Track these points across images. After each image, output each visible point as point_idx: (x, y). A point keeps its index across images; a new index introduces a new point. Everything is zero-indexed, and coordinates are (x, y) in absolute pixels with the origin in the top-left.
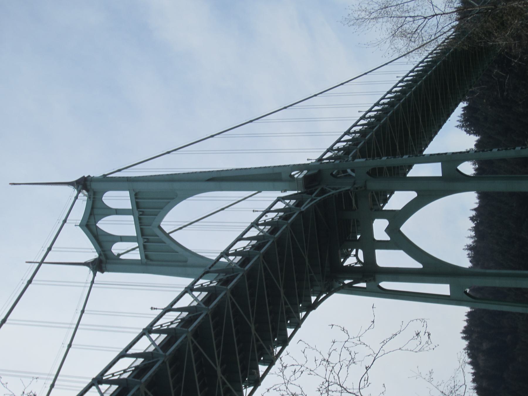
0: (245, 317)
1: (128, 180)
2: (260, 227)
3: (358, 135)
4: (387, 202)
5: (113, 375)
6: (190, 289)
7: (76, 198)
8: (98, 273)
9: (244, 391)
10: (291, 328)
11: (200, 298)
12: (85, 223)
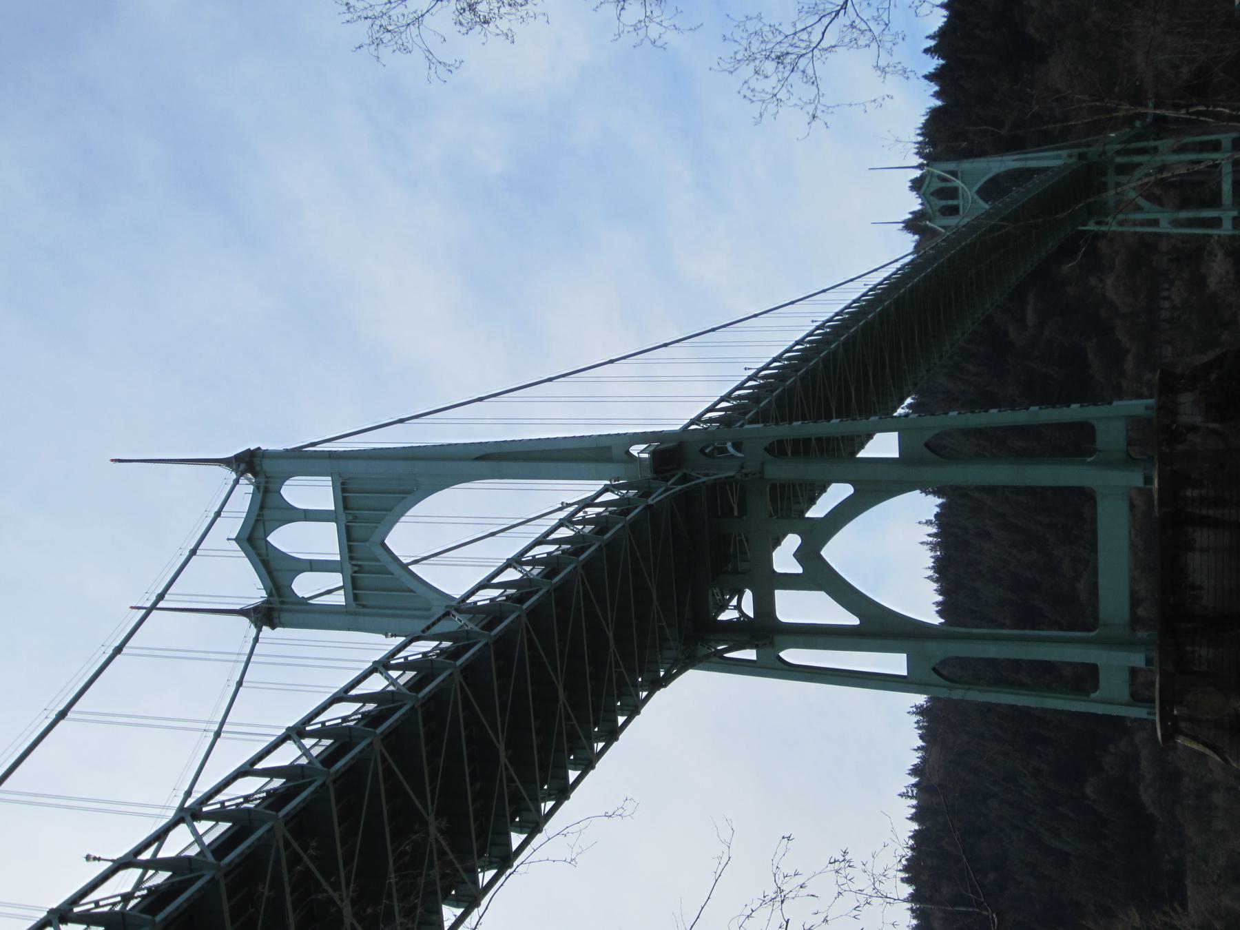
0: (416, 801)
1: (331, 455)
2: (391, 673)
3: (589, 528)
4: (567, 798)
5: (97, 904)
6: (382, 666)
7: (256, 640)
8: (265, 629)
9: (481, 875)
10: (575, 769)
11: (315, 752)
12: (246, 536)
